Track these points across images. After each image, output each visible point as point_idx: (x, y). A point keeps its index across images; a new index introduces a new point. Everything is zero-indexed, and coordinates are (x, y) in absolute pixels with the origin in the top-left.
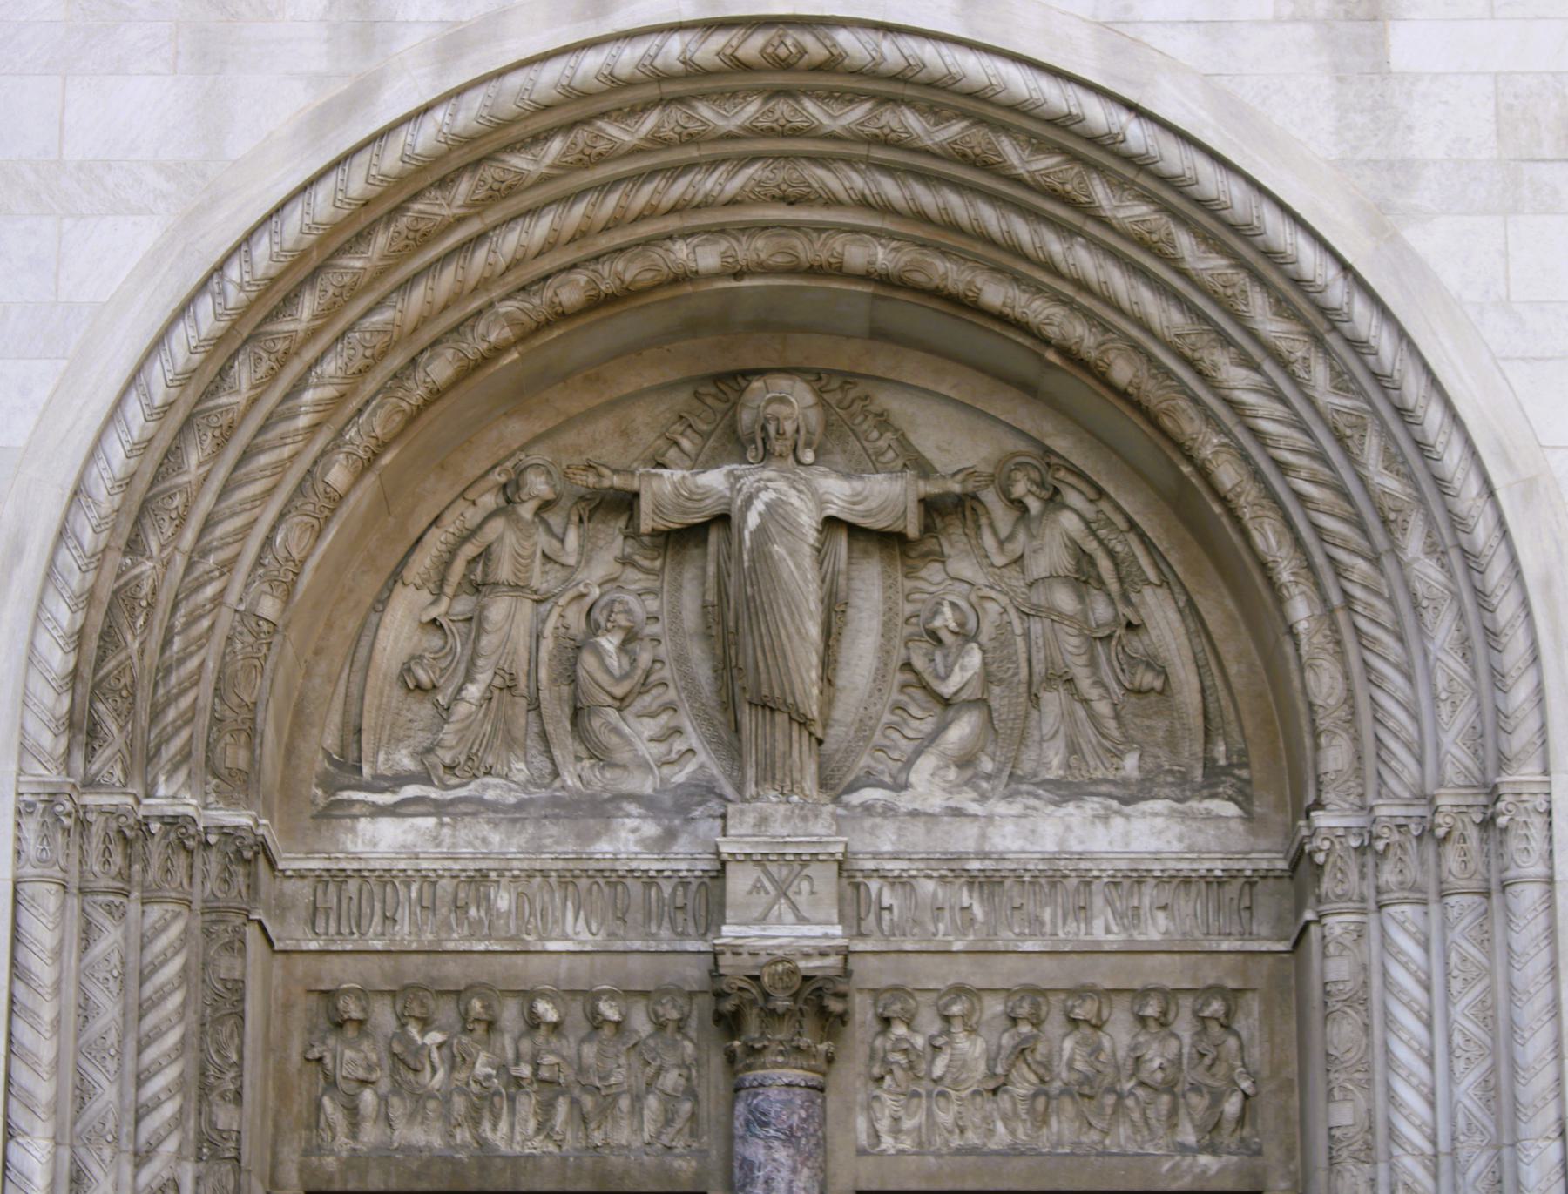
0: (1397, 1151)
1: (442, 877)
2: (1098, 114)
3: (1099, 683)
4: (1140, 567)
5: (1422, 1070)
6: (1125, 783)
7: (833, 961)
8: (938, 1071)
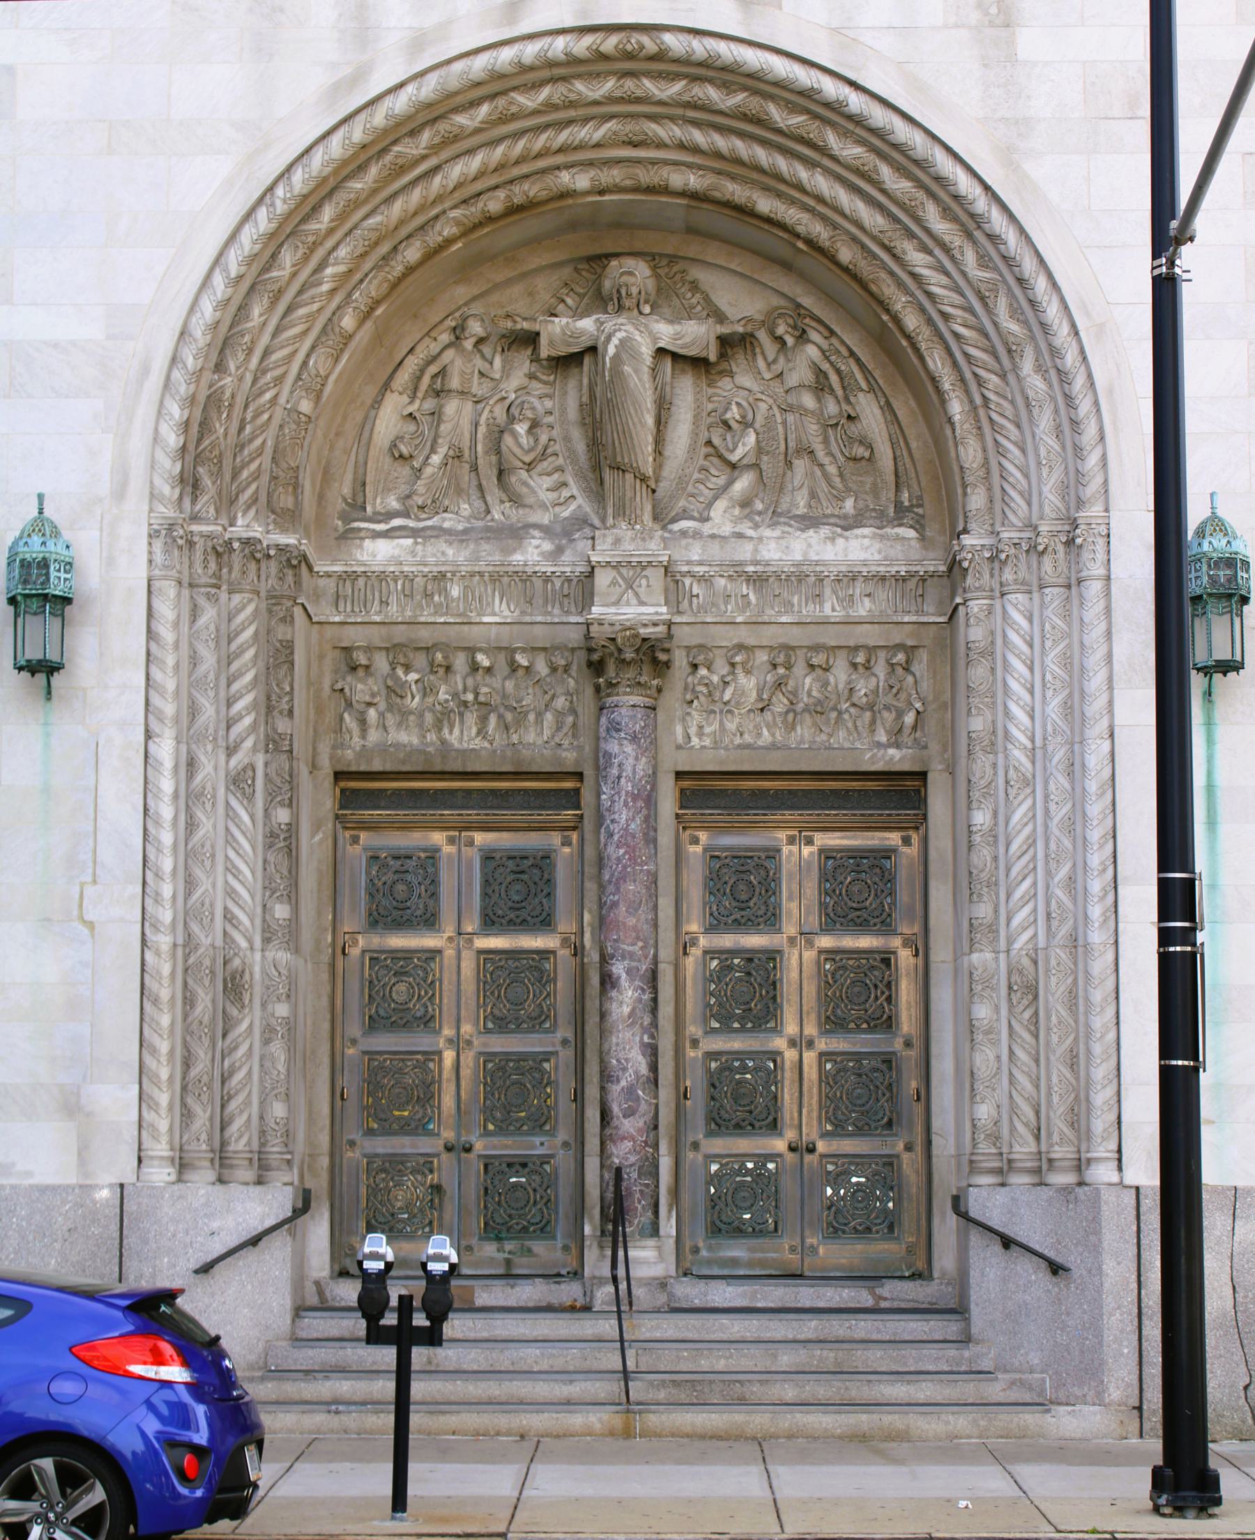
0: (1010, 746)
3: (830, 454)
6: (845, 517)
7: (661, 629)
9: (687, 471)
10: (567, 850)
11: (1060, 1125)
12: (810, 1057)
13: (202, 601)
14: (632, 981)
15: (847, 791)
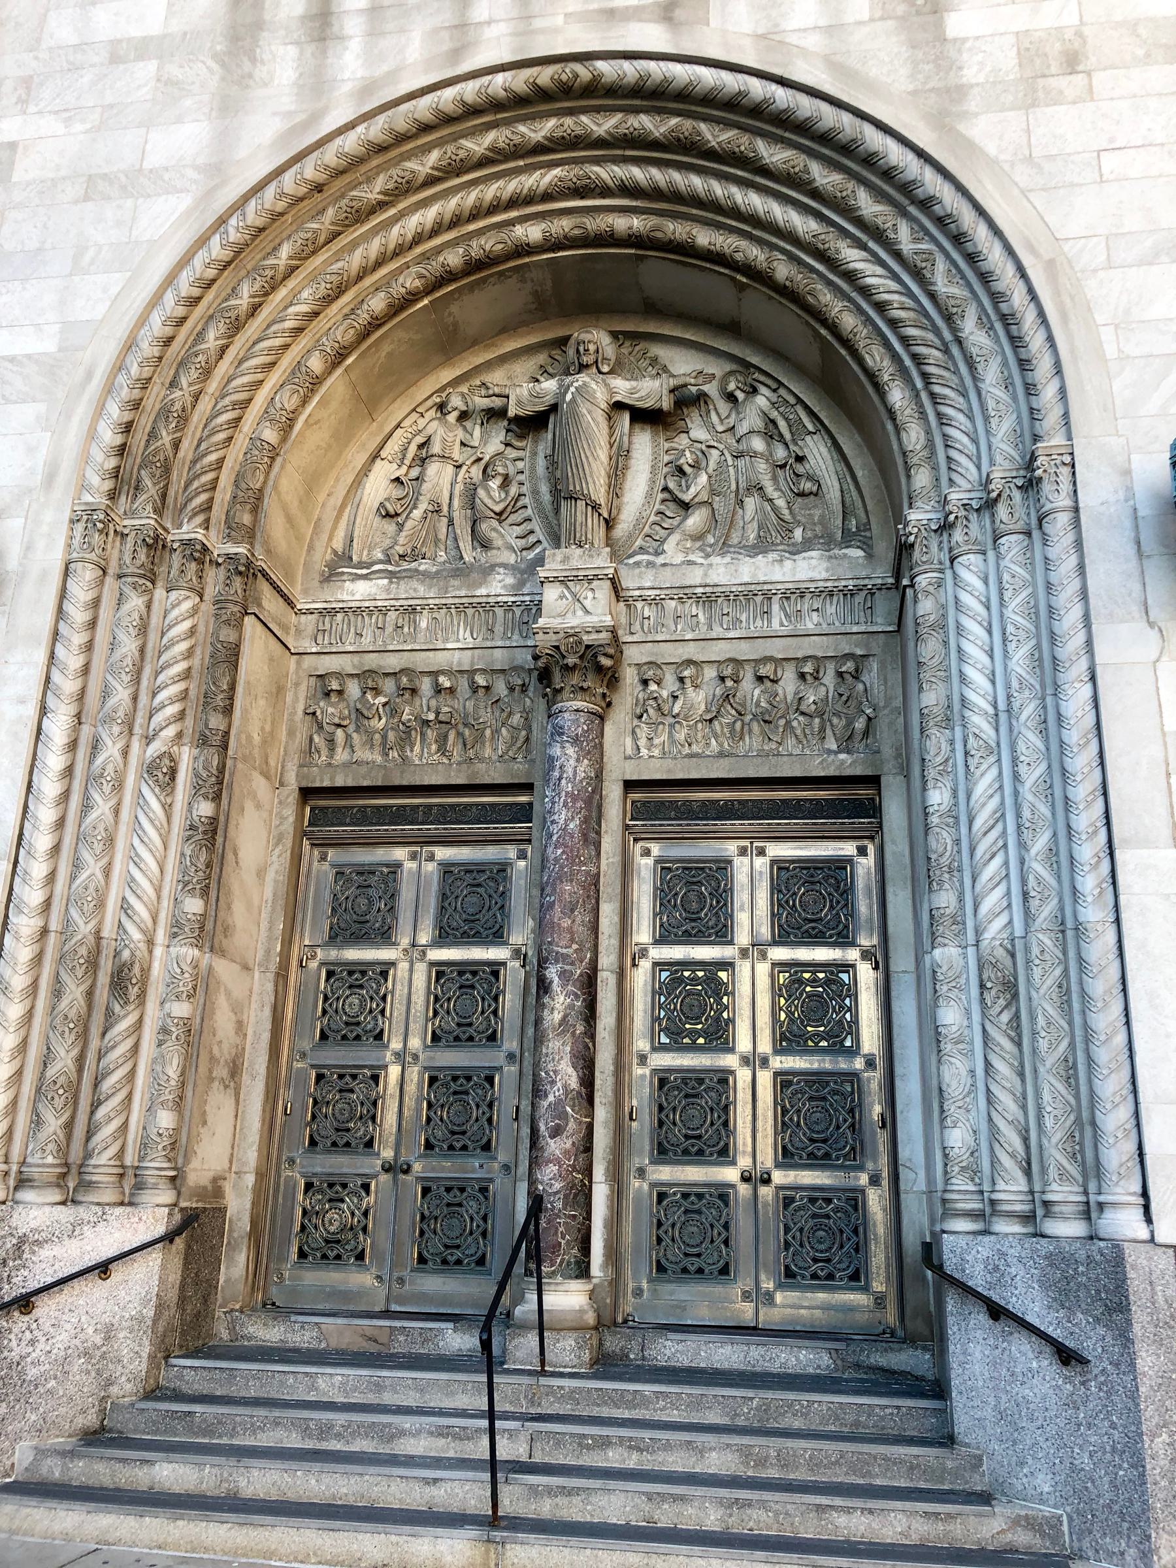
0: (968, 713)
2: (757, 89)
3: (778, 489)
5: (985, 659)
6: (794, 545)
7: (604, 636)
8: (676, 710)
9: (644, 514)
10: (522, 864)
11: (1057, 1156)
12: (765, 1078)
13: (127, 590)
14: (563, 986)
15: (799, 801)
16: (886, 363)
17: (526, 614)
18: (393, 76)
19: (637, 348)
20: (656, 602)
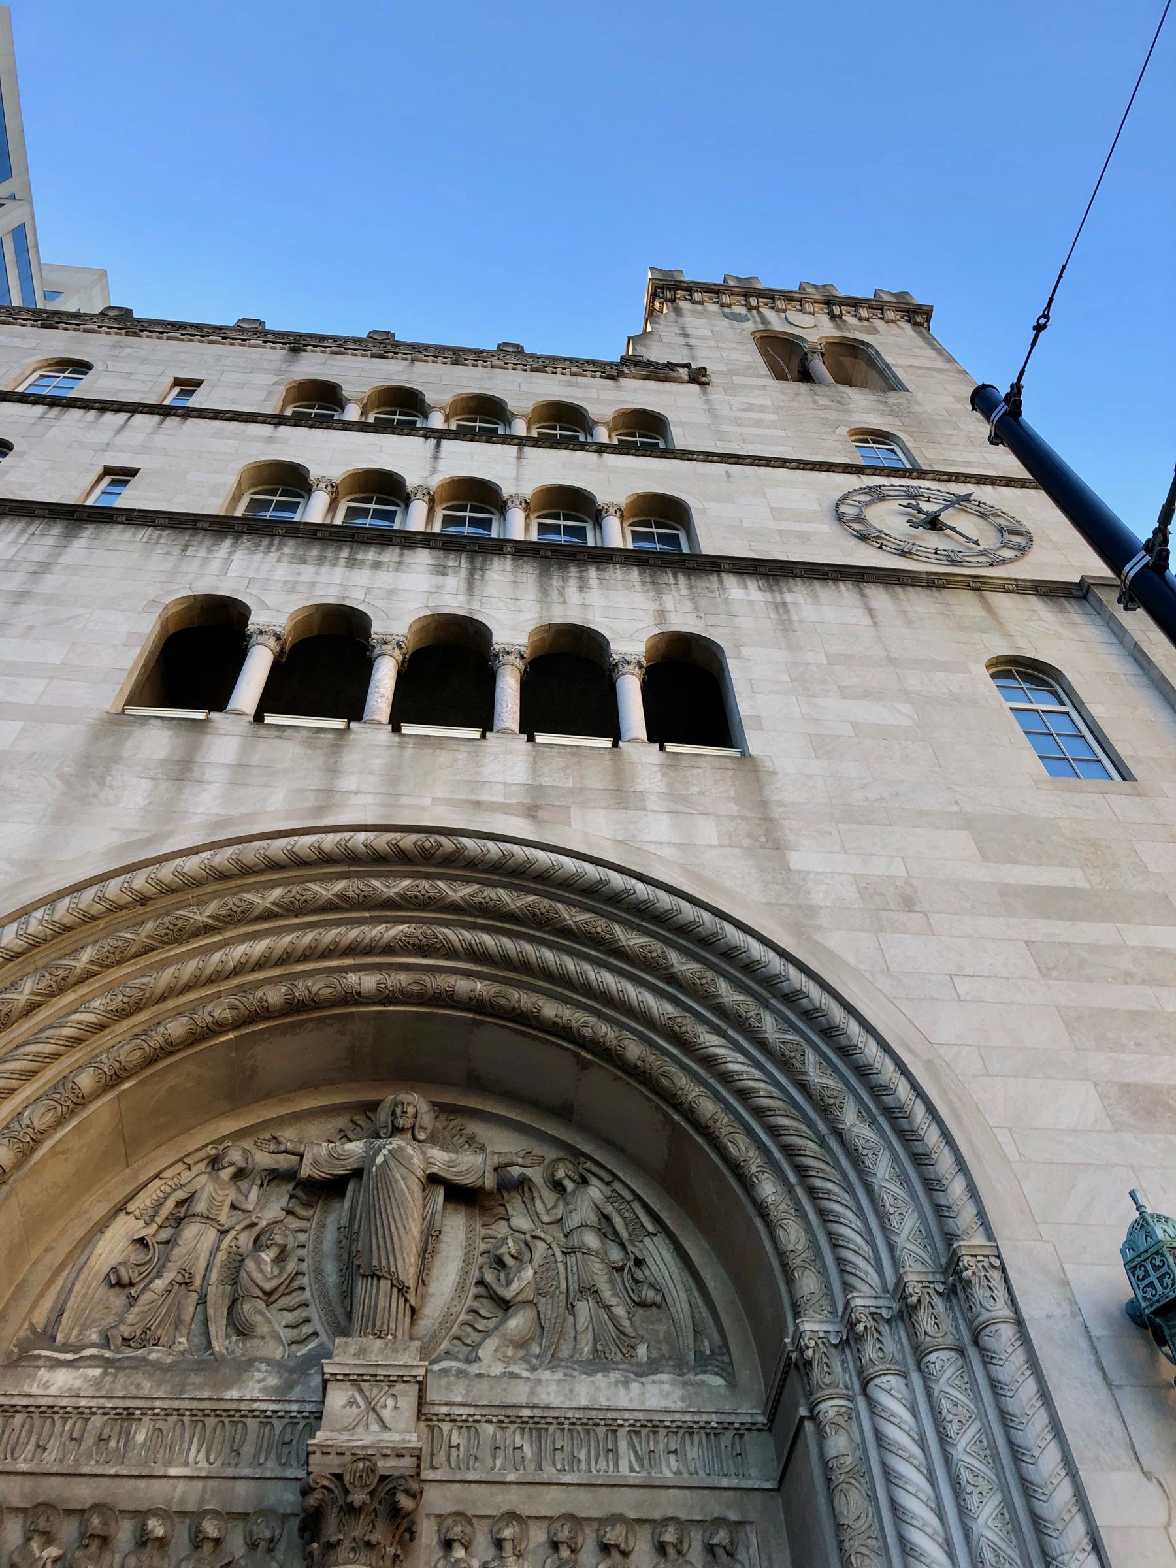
1: (95, 1413)
2: (618, 880)
3: (615, 1294)
4: (642, 1225)
7: (408, 1462)
9: (454, 1310)
16: (753, 1153)
17: (289, 1430)
18: (248, 818)
19: (453, 1124)
20: (468, 1425)
